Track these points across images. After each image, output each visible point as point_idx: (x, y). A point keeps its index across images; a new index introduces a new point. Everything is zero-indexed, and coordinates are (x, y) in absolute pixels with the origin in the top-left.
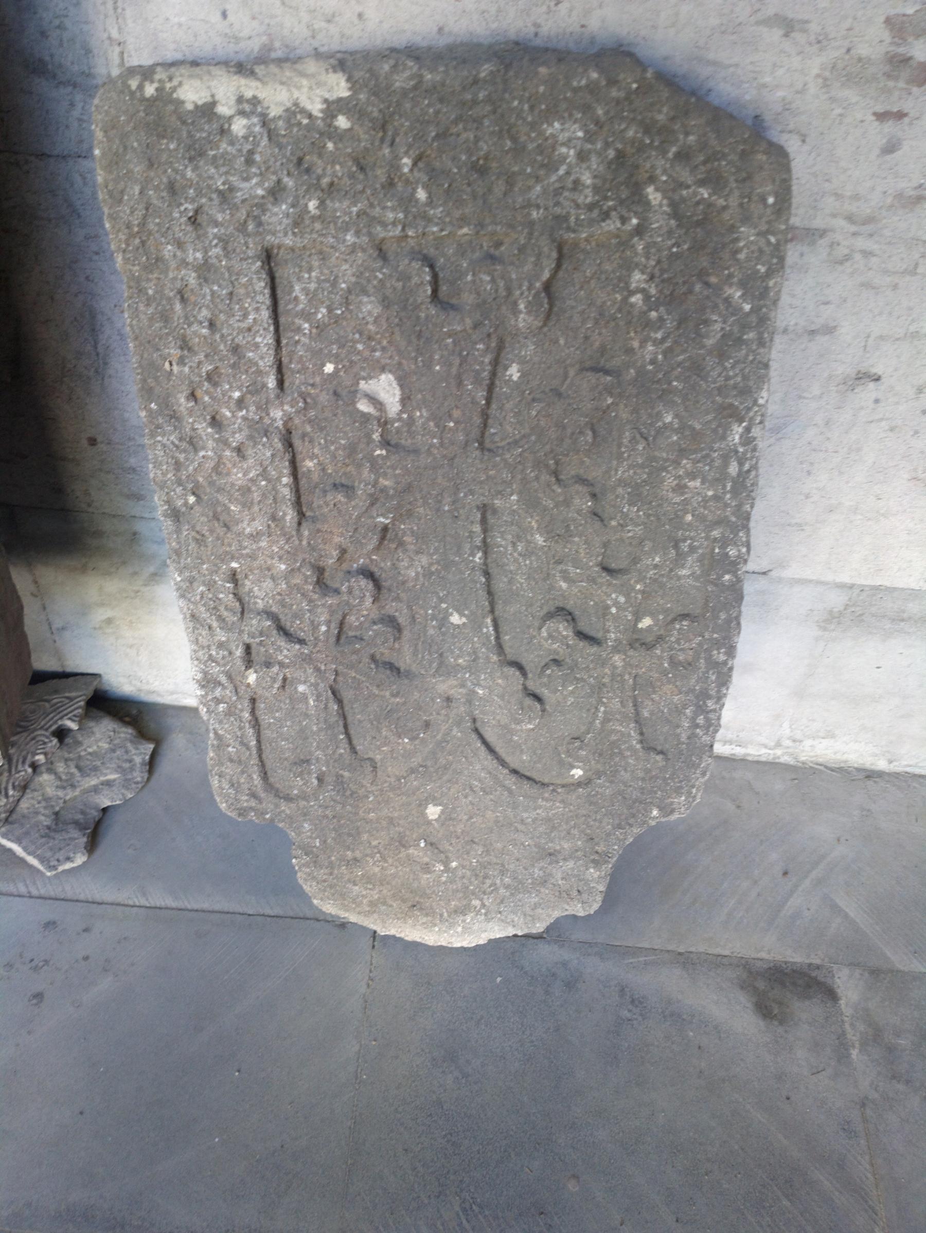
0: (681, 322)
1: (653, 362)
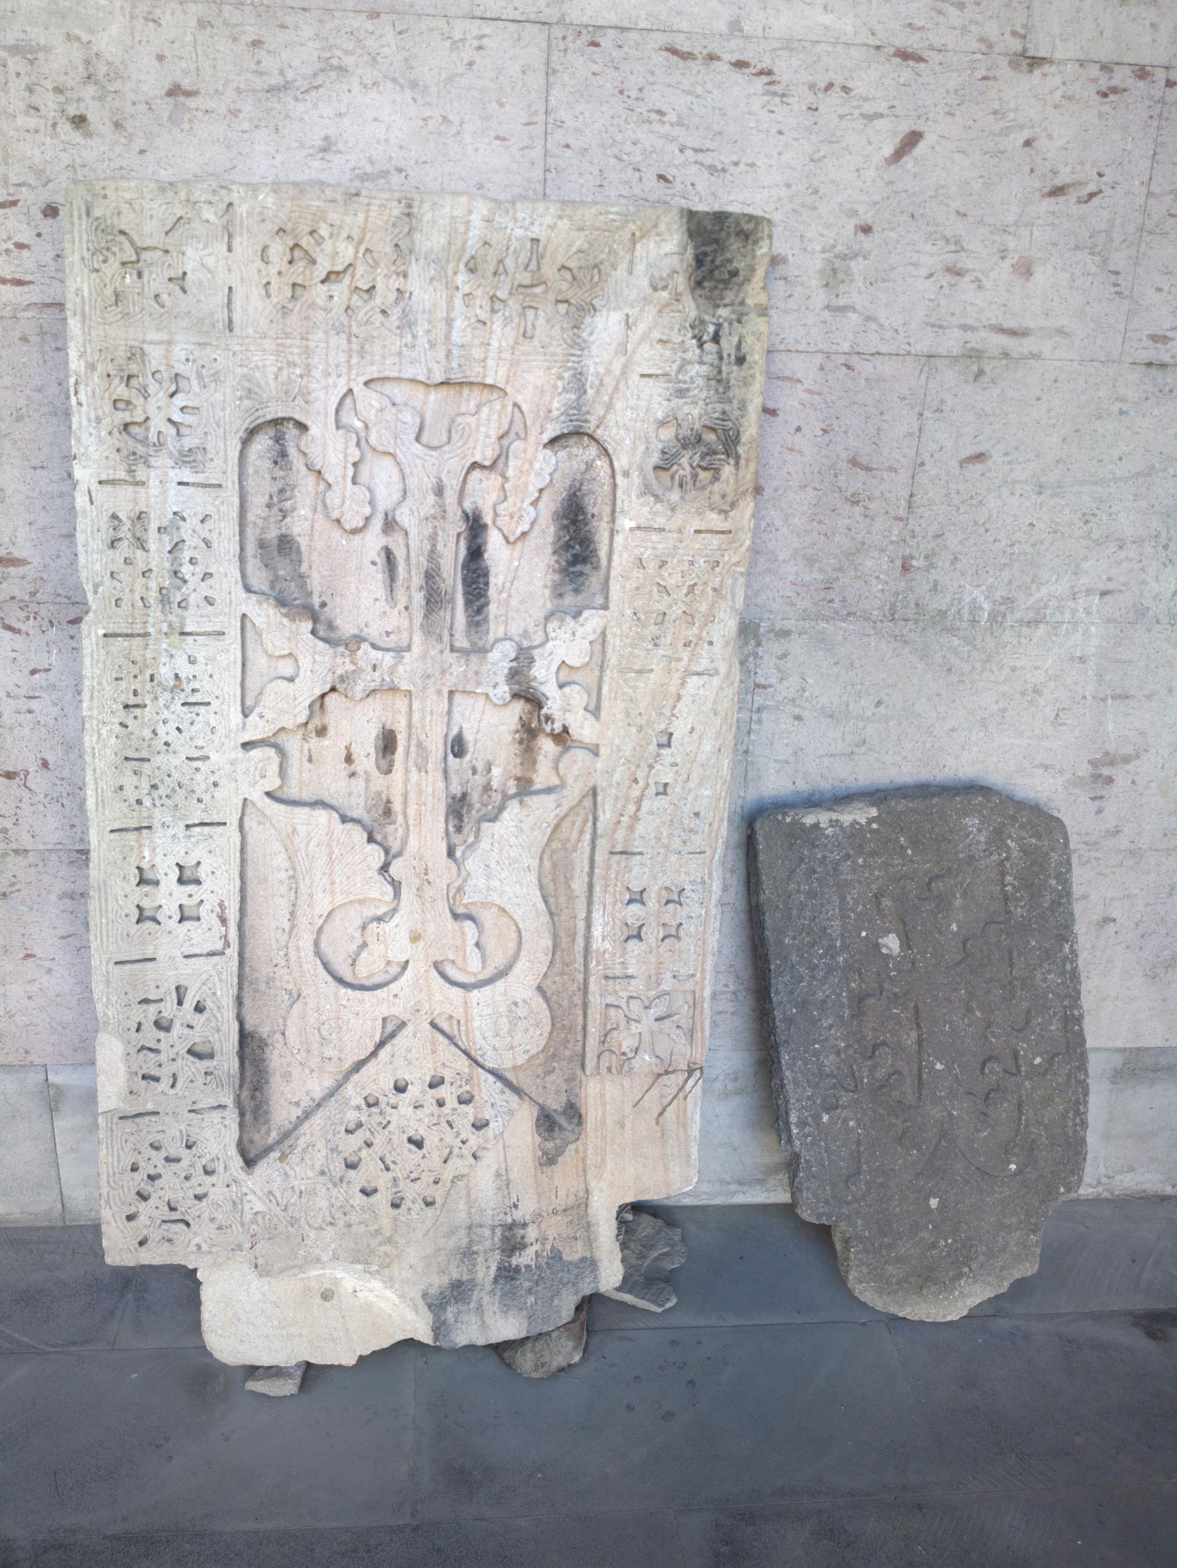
0: (1032, 896)
1: (1022, 916)
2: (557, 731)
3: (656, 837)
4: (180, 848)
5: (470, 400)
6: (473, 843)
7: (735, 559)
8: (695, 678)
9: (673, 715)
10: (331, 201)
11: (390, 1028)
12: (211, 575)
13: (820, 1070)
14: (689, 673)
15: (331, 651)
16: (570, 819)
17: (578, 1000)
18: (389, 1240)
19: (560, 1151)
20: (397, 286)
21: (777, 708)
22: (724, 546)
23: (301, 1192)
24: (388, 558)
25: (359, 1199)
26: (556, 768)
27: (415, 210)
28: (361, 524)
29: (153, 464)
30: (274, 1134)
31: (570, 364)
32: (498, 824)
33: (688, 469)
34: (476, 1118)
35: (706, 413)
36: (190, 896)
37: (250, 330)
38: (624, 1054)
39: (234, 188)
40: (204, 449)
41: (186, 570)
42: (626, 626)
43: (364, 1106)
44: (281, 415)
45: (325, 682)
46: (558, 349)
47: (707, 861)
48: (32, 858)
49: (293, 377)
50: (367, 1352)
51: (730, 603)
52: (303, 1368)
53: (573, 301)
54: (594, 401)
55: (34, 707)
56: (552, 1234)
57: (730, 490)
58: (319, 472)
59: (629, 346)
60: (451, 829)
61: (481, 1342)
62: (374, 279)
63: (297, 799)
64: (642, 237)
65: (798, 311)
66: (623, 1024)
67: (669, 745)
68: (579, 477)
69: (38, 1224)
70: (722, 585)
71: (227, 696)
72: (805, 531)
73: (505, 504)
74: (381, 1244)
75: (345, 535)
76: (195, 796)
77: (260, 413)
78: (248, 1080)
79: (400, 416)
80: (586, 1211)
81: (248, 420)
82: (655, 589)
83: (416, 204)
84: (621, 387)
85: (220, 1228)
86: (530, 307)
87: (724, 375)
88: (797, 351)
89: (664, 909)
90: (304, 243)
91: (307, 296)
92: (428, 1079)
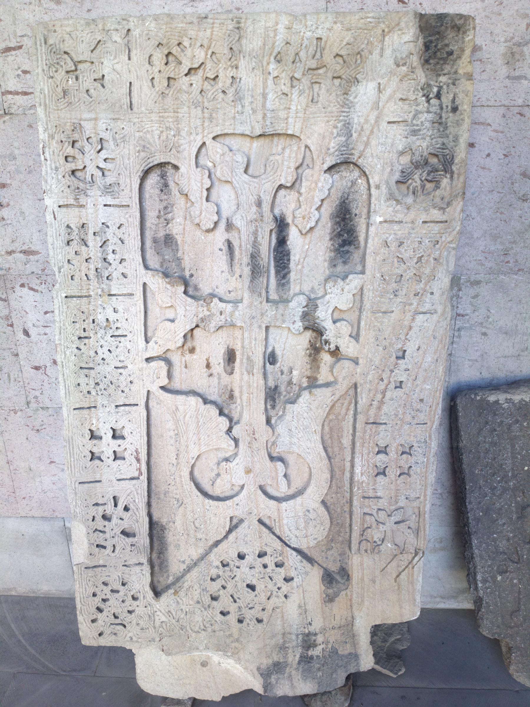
2: (332, 350)
3: (395, 414)
4: (113, 419)
5: (279, 144)
6: (282, 416)
7: (449, 239)
8: (421, 316)
9: (406, 339)
10: (190, 23)
11: (235, 521)
12: (125, 259)
13: (496, 550)
14: (417, 313)
15: (196, 304)
16: (341, 401)
17: (346, 509)
18: (237, 640)
19: (336, 595)
20: (231, 75)
21: (471, 328)
22: (442, 231)
23: (186, 612)
24: (229, 246)
25: (220, 617)
26: (332, 371)
27: (242, 25)
28: (212, 226)
29: (89, 194)
30: (171, 578)
31: (341, 118)
32: (296, 405)
33: (419, 182)
34: (286, 575)
35: (431, 145)
36: (119, 446)
37: (143, 109)
38: (375, 542)
39: (131, 19)
40: (119, 184)
41: (110, 257)
42: (376, 285)
43: (221, 566)
44: (163, 161)
45: (192, 322)
46: (334, 109)
47: (428, 429)
48: (50, 411)
49: (170, 137)
50: (227, 695)
51: (445, 267)
52: (192, 700)
53: (344, 77)
54: (357, 141)
55: (47, 332)
56: (332, 640)
57: (446, 194)
58: (187, 195)
59: (381, 104)
60: (269, 407)
61: (291, 694)
62: (217, 71)
63: (179, 389)
64: (389, 32)
65: (489, 80)
66: (374, 525)
67: (403, 357)
68: (347, 190)
69: (64, 596)
70: (440, 256)
71: (136, 331)
72: (492, 219)
73: (300, 210)
74: (232, 642)
75: (203, 234)
76: (120, 389)
77: (151, 160)
78: (156, 548)
79: (235, 157)
80: (352, 628)
81: (144, 165)
82: (396, 260)
83: (243, 20)
84: (375, 130)
85: (142, 629)
86: (316, 82)
87: (444, 120)
88: (488, 106)
89: (400, 458)
90: (174, 51)
91: (176, 85)
92: (257, 553)
